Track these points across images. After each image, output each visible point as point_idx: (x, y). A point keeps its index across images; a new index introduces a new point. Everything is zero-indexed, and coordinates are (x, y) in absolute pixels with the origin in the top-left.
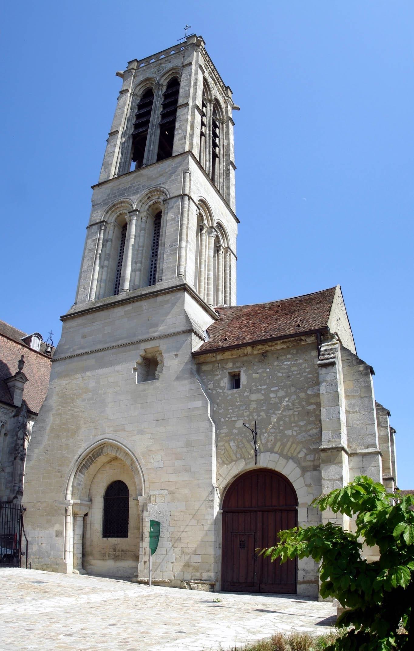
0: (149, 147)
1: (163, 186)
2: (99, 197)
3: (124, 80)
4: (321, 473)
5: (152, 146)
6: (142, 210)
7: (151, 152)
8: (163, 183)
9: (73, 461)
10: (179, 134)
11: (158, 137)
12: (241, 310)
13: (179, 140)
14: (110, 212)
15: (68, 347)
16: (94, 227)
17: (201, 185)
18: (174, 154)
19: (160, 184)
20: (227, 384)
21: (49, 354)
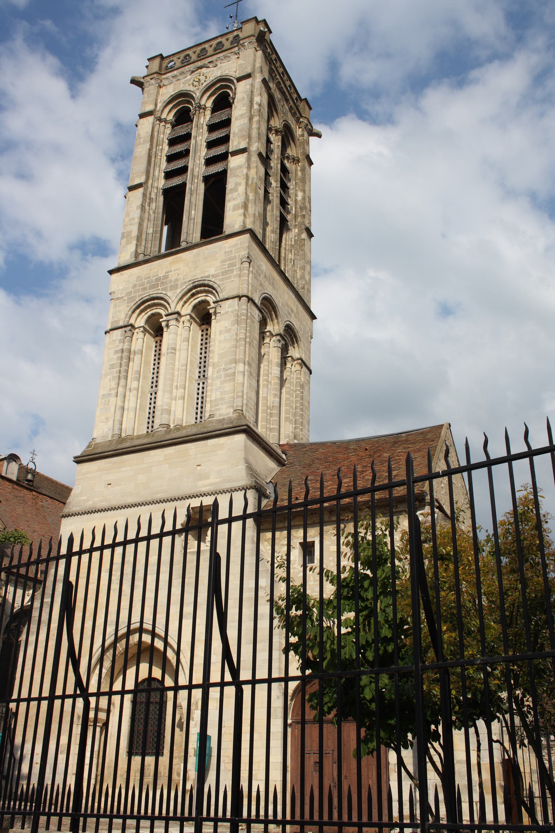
0: (190, 213)
1: (213, 280)
2: (121, 287)
3: (143, 89)
4: (502, 57)
5: (193, 212)
6: (183, 313)
7: (192, 221)
8: (213, 276)
9: (352, 756)
10: (234, 199)
11: (202, 197)
12: (317, 450)
13: (234, 210)
14: (138, 311)
15: (85, 498)
16: (115, 332)
17: (265, 276)
18: (227, 230)
19: (208, 276)
20: (297, 558)
21: (31, 483)
